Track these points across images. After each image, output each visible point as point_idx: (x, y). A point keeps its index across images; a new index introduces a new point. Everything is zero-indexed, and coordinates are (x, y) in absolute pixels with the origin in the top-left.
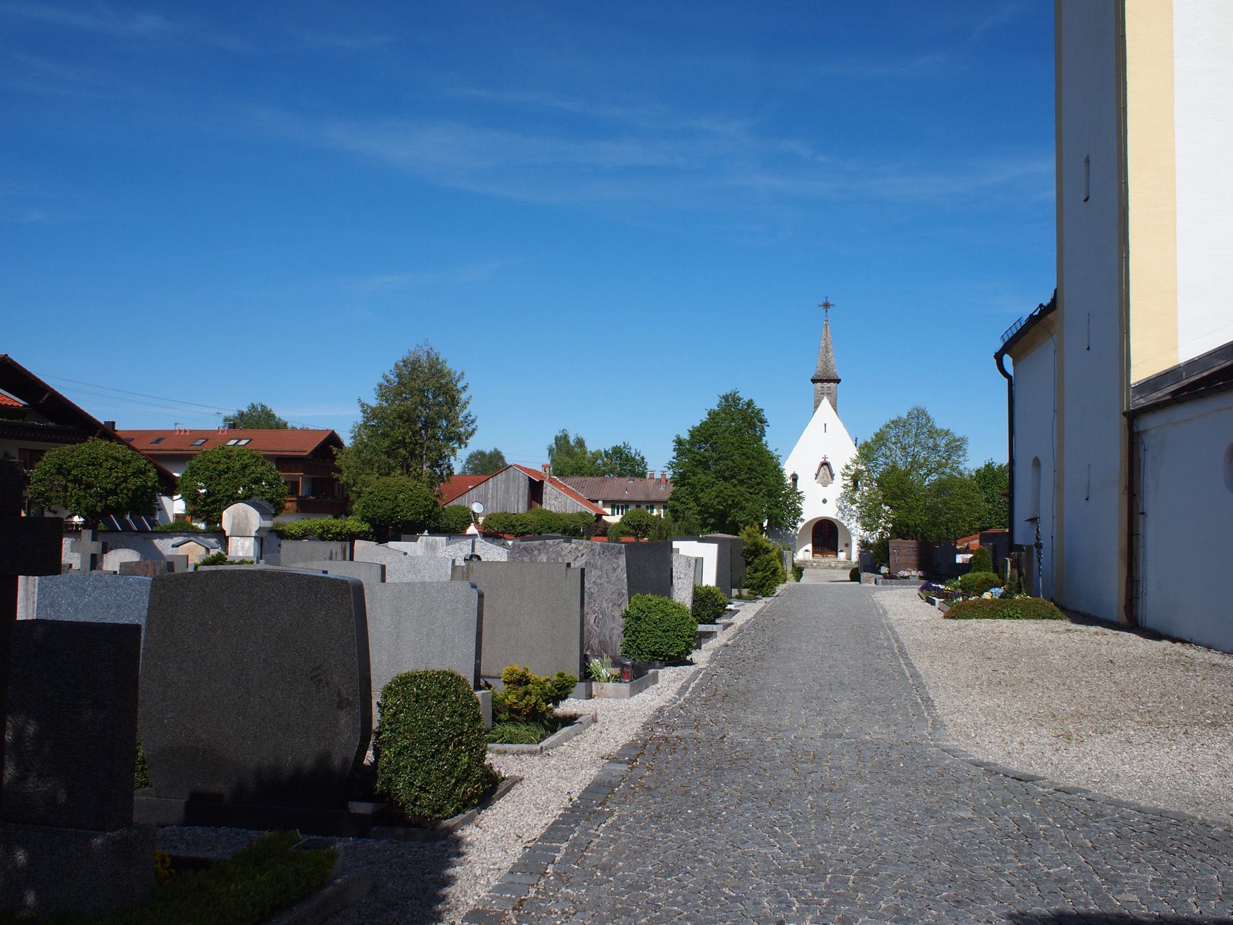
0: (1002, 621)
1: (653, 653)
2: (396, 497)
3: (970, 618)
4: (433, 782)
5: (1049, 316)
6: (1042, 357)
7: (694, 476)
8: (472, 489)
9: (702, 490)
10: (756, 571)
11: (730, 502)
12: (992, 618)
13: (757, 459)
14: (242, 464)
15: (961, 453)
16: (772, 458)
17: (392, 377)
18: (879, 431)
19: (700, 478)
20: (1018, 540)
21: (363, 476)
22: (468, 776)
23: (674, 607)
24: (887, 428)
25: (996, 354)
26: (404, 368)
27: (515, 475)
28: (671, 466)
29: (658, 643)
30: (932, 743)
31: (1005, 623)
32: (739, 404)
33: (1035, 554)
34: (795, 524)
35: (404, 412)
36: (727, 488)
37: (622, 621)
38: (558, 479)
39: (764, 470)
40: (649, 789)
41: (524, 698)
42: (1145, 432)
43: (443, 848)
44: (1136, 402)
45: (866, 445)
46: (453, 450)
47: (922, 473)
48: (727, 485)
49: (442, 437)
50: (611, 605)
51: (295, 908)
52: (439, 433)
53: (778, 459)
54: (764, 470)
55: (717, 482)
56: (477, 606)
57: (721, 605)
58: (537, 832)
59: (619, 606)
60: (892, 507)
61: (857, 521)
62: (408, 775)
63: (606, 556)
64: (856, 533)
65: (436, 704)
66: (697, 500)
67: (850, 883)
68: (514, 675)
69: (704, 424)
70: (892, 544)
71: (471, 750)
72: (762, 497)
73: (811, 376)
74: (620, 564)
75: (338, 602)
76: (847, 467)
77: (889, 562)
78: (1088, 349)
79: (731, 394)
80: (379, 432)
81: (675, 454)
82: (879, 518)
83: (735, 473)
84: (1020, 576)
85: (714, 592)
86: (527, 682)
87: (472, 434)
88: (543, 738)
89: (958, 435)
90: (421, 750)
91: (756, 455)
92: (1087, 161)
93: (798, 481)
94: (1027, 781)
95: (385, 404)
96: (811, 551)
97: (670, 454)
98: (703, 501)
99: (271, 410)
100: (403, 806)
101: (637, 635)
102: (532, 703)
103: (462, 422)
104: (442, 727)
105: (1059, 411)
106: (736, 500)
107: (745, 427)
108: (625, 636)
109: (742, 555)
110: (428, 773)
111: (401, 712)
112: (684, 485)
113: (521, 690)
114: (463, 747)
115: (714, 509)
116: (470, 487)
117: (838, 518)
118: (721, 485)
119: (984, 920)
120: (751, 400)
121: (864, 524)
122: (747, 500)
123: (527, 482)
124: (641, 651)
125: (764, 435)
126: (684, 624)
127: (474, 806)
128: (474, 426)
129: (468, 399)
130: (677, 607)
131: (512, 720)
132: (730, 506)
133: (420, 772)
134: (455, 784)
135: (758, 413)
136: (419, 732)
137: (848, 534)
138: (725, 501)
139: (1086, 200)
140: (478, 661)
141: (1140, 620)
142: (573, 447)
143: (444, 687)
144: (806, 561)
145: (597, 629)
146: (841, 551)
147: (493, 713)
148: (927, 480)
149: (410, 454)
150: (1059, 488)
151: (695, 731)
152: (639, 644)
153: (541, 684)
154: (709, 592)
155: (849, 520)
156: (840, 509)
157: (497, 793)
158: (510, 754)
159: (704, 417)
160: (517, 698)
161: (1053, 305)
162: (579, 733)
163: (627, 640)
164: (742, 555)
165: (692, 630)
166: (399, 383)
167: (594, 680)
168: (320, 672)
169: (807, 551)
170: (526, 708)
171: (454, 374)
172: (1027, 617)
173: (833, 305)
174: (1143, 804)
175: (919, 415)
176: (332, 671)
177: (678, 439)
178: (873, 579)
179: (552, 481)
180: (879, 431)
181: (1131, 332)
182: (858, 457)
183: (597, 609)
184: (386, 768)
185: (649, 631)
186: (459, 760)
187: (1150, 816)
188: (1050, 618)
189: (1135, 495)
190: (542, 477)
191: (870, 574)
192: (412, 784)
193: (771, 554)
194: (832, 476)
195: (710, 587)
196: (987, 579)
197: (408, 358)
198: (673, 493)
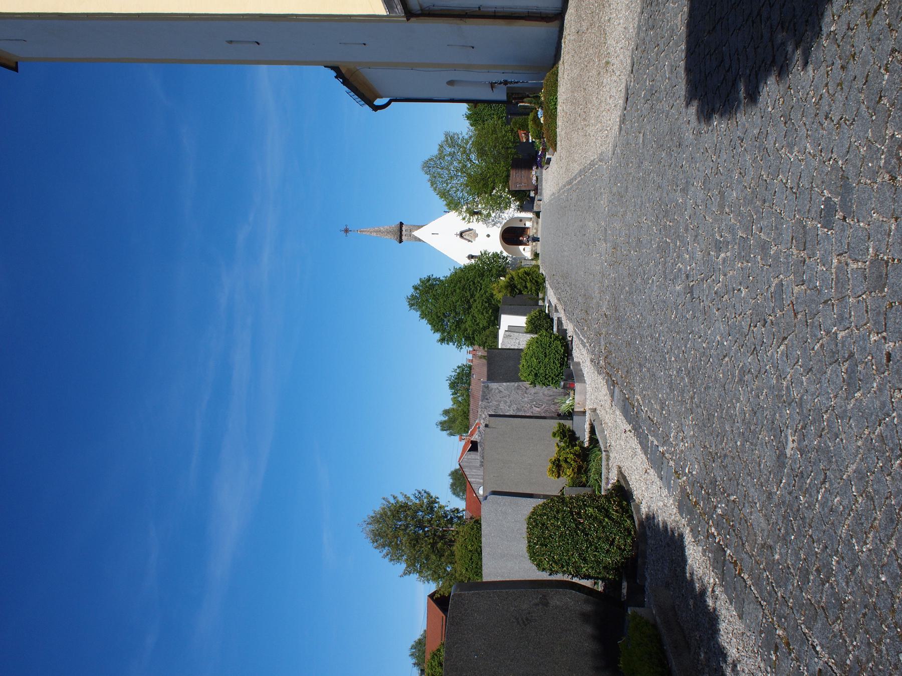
0: (558, 110)
1: (562, 365)
2: (470, 551)
3: (556, 133)
4: (606, 535)
5: (343, 71)
6: (374, 77)
7: (467, 330)
8: (476, 494)
9: (478, 324)
10: (526, 287)
11: (487, 305)
12: (556, 117)
13: (456, 284)
14: (438, 667)
15: (456, 137)
16: (456, 273)
17: (385, 551)
18: (438, 196)
19: (469, 326)
20: (504, 97)
21: (457, 575)
22: (604, 509)
23: (529, 348)
24: (436, 190)
25: (373, 110)
26: (378, 542)
27: (466, 462)
28: (459, 346)
29: (554, 361)
30: (610, 162)
31: (559, 108)
32: (416, 296)
33: (512, 85)
34: (504, 257)
35: (410, 543)
36: (477, 306)
37: (538, 387)
38: (471, 430)
39: (464, 279)
40: (627, 372)
41: (569, 463)
42: (421, 6)
43: (651, 529)
44: (400, 11)
45: (448, 205)
46: (440, 507)
47: (469, 165)
48: (474, 306)
49: (431, 516)
50: (526, 395)
51: (665, 648)
52: (428, 517)
53: (456, 269)
54: (464, 279)
55: (472, 313)
56: (500, 496)
57: (540, 314)
58: (644, 458)
59: (527, 389)
60: (494, 189)
61: (503, 213)
62: (601, 554)
63: (490, 397)
64: (512, 214)
65: (549, 531)
66: (484, 329)
67: (671, 224)
68: (554, 470)
69: (431, 322)
70: (513, 188)
71: (585, 505)
72: (484, 281)
73: (397, 243)
74: (496, 387)
75: (468, 603)
76: (464, 219)
77: (526, 190)
78: (365, 44)
79: (409, 302)
80: (425, 562)
81: (451, 344)
82: (501, 197)
83: (465, 300)
84: (529, 97)
85: (530, 318)
86: (559, 460)
87: (428, 494)
88: (600, 450)
89: (443, 138)
90: (582, 543)
91: (452, 285)
92: (231, 42)
93: (473, 255)
94: (628, 93)
95: (405, 557)
96: (524, 246)
97: (451, 347)
98: (486, 324)
99: (415, 642)
100: (625, 559)
101: (548, 376)
102: (573, 457)
103: (420, 500)
104: (565, 527)
105: (412, 66)
106: (485, 300)
107: (432, 292)
108: (549, 385)
109: (514, 297)
110: (599, 538)
111: (553, 557)
112: (474, 338)
113: (564, 464)
114: (582, 511)
115: (491, 316)
116: (475, 495)
117: (501, 226)
118: (474, 311)
119: (688, 126)
120: (413, 287)
121: (506, 208)
122: (486, 292)
123: (471, 452)
124: (560, 374)
125: (439, 278)
126: (541, 341)
127: (629, 504)
128: (423, 492)
129: (403, 495)
130: (530, 345)
131: (587, 471)
132: (489, 304)
133: (599, 545)
134: (610, 518)
135: (423, 282)
136: (569, 544)
137: (512, 219)
138: (486, 308)
139: (258, 44)
140: (542, 497)
141: (557, 12)
142: (449, 418)
143: (537, 524)
144: (532, 250)
145: (543, 406)
146: (525, 225)
147: (581, 486)
148: (474, 161)
149: (442, 539)
150: (468, 67)
151: (603, 336)
152: (555, 375)
153: (561, 449)
154: (530, 322)
155: (503, 219)
156: (494, 225)
157: (624, 486)
158: (609, 475)
159: (424, 322)
160: (569, 468)
161: (335, 69)
162: (600, 422)
163: (552, 383)
164: (514, 297)
165: (546, 336)
166: (389, 546)
167: (573, 409)
168: (520, 619)
169: (524, 250)
170: (577, 462)
171: (384, 505)
172: (556, 92)
173: (346, 226)
174: (639, 10)
175: (428, 166)
176: (520, 609)
177: (440, 341)
178: (538, 202)
179: (472, 434)
180: (438, 196)
181: (349, 14)
182: (457, 211)
183: (529, 405)
184: (596, 571)
185: (545, 367)
186: (592, 515)
187: (645, 5)
188: (557, 76)
189: (467, 13)
190: (468, 441)
191: (535, 204)
192: (608, 551)
193: (514, 276)
194: (470, 230)
195: (526, 321)
196: (532, 120)
197: (371, 539)
198: (480, 345)
